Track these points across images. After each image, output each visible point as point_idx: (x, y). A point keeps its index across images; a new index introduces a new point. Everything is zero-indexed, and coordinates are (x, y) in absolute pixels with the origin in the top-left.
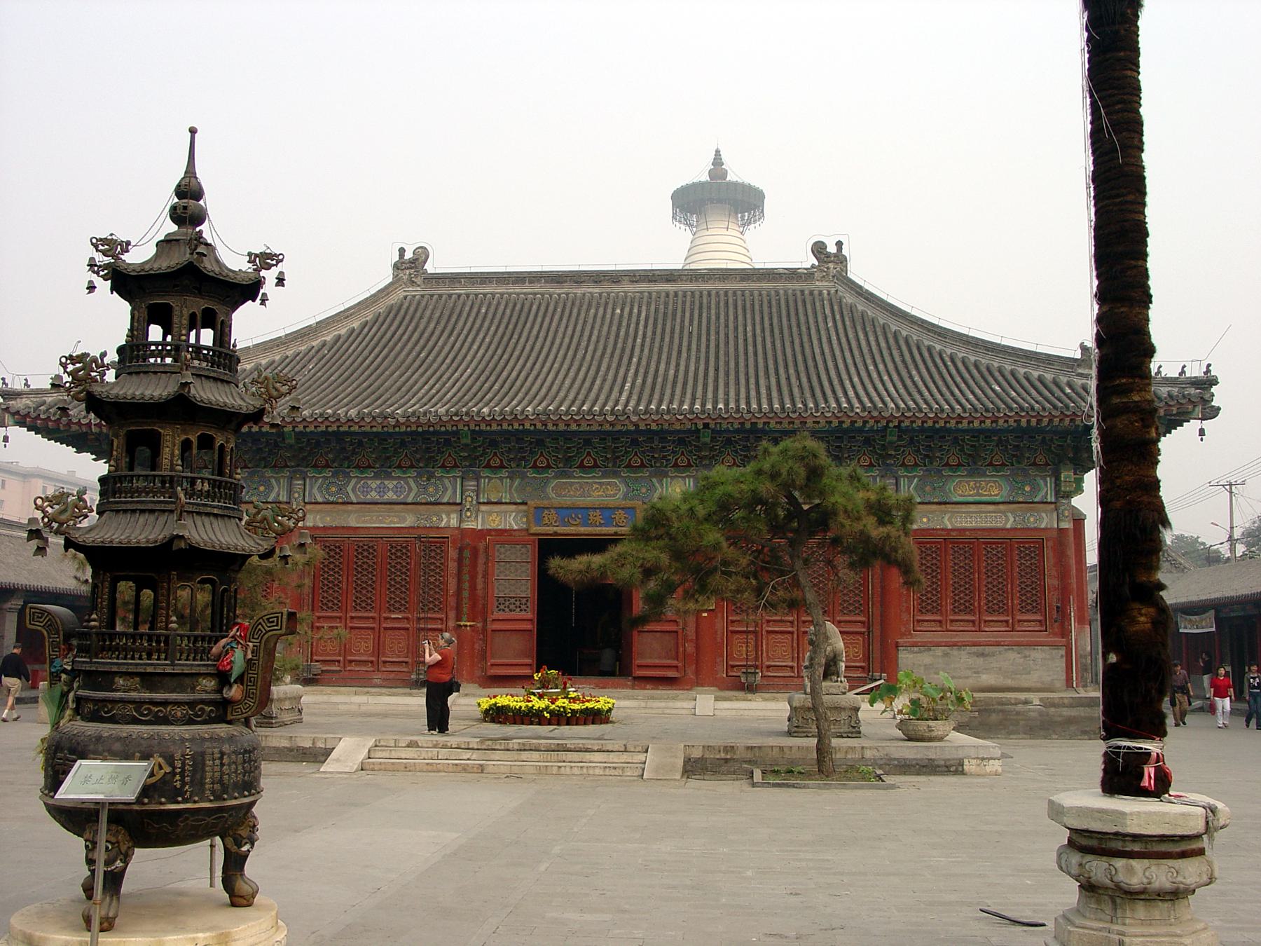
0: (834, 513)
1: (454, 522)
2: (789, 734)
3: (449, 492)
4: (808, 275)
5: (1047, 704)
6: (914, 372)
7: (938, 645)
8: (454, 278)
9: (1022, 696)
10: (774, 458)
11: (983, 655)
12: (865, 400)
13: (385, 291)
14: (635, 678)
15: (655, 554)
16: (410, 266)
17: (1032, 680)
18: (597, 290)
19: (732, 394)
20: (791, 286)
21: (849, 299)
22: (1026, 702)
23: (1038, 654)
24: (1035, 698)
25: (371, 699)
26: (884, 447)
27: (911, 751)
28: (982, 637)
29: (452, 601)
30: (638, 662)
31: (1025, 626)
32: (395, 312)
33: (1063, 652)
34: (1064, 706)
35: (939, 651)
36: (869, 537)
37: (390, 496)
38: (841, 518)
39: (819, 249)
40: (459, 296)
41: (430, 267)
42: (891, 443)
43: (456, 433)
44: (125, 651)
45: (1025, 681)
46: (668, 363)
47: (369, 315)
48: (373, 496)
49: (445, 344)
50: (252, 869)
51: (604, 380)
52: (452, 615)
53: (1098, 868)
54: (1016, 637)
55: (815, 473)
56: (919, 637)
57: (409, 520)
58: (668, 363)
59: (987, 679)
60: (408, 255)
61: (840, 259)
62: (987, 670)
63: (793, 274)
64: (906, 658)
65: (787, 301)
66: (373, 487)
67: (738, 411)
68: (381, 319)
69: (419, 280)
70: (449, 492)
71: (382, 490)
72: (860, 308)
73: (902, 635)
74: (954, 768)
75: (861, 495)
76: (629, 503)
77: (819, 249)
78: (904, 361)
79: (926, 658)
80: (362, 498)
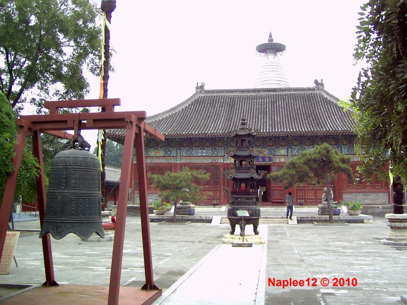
0: (333, 162)
1: (222, 161)
2: (322, 214)
3: (220, 153)
4: (313, 89)
5: (384, 208)
6: (345, 119)
7: (353, 192)
8: (213, 91)
9: (377, 206)
10: (319, 149)
11: (366, 195)
12: (333, 128)
13: (194, 95)
14: (272, 202)
15: (293, 172)
16: (200, 88)
17: (380, 201)
18: (254, 94)
19: (296, 126)
20: (309, 92)
21: (325, 96)
22: (378, 207)
23: (381, 195)
24: (380, 206)
25: (204, 209)
26: (338, 140)
27: (351, 218)
28: (365, 190)
29: (222, 182)
30: (273, 198)
31: (377, 187)
32: (197, 101)
33: (387, 194)
34: (388, 208)
35: (354, 194)
36: (341, 167)
37: (204, 154)
38: (335, 163)
39: (316, 82)
40: (215, 96)
41: (206, 88)
42: (340, 139)
43: (223, 138)
44: (252, 195)
45: (377, 202)
46: (277, 117)
47: (190, 102)
48: (200, 154)
49: (214, 111)
50: (258, 229)
51: (261, 122)
52: (222, 186)
53: (393, 224)
54: (375, 190)
55: (328, 152)
56: (348, 190)
57: (210, 161)
58: (277, 117)
59: (367, 201)
60: (199, 85)
61: (322, 85)
62: (367, 199)
63: (309, 89)
64: (345, 196)
65: (308, 97)
66: (199, 152)
67: (299, 131)
68: (194, 104)
69: (203, 92)
70: (220, 153)
71: (202, 153)
72: (329, 99)
73: (344, 190)
74: (362, 221)
75: (338, 156)
76: (270, 156)
77: (316, 82)
78: (342, 115)
79: (350, 196)
80: (197, 155)
